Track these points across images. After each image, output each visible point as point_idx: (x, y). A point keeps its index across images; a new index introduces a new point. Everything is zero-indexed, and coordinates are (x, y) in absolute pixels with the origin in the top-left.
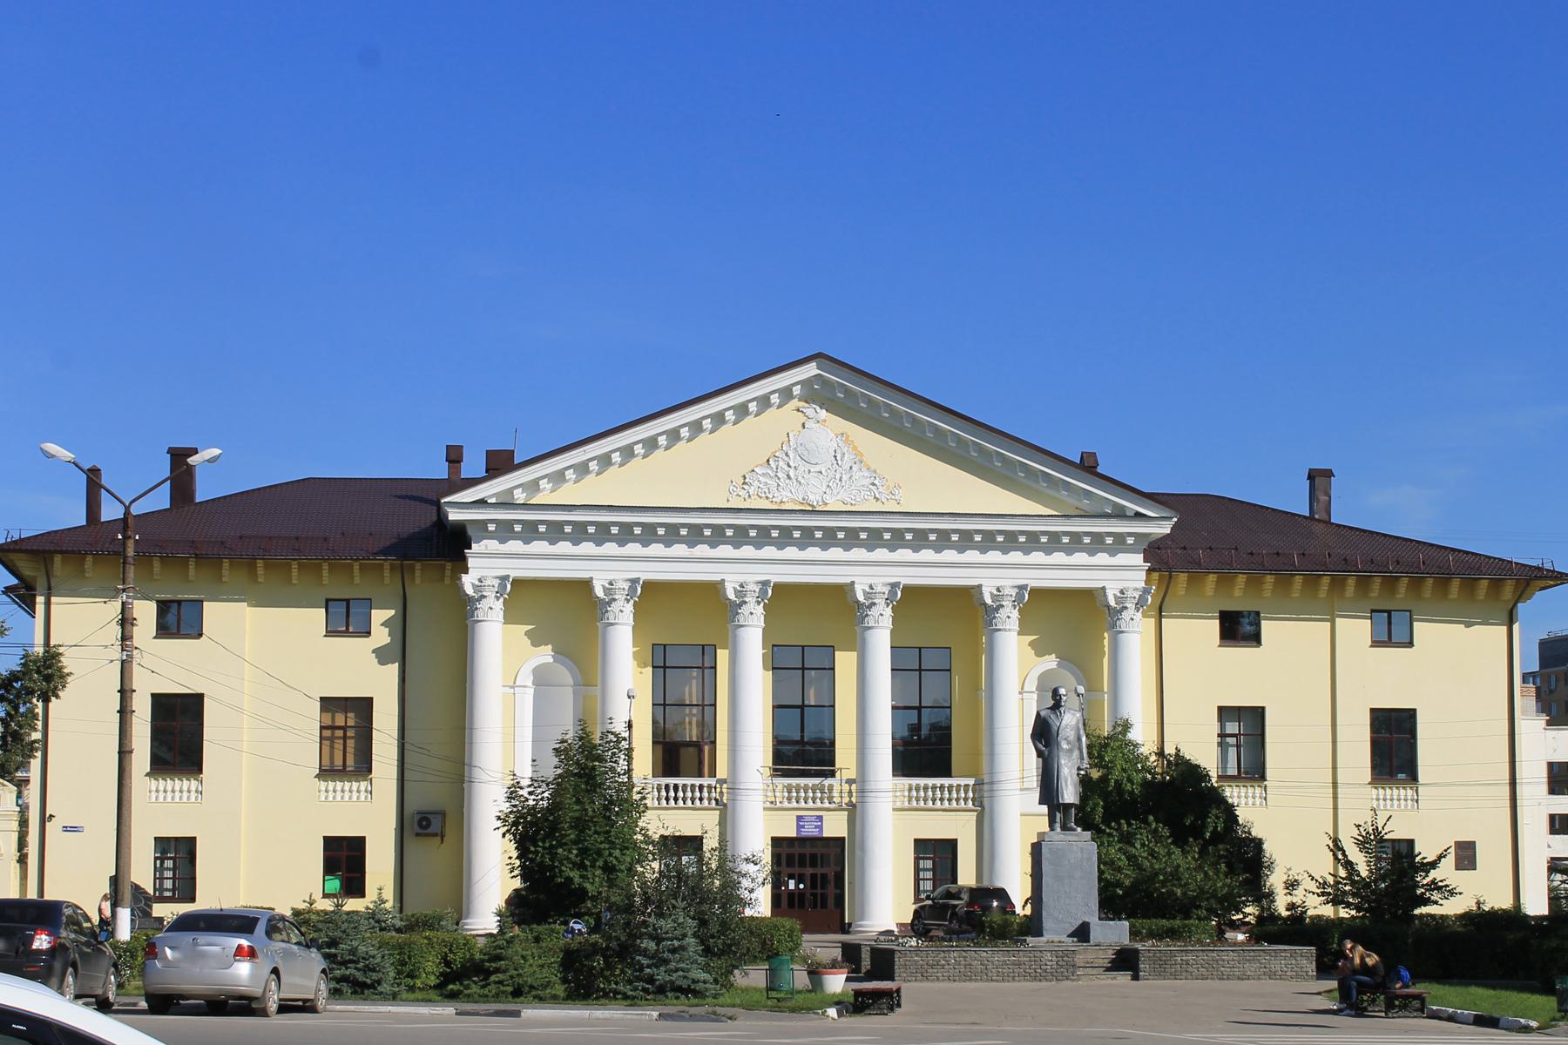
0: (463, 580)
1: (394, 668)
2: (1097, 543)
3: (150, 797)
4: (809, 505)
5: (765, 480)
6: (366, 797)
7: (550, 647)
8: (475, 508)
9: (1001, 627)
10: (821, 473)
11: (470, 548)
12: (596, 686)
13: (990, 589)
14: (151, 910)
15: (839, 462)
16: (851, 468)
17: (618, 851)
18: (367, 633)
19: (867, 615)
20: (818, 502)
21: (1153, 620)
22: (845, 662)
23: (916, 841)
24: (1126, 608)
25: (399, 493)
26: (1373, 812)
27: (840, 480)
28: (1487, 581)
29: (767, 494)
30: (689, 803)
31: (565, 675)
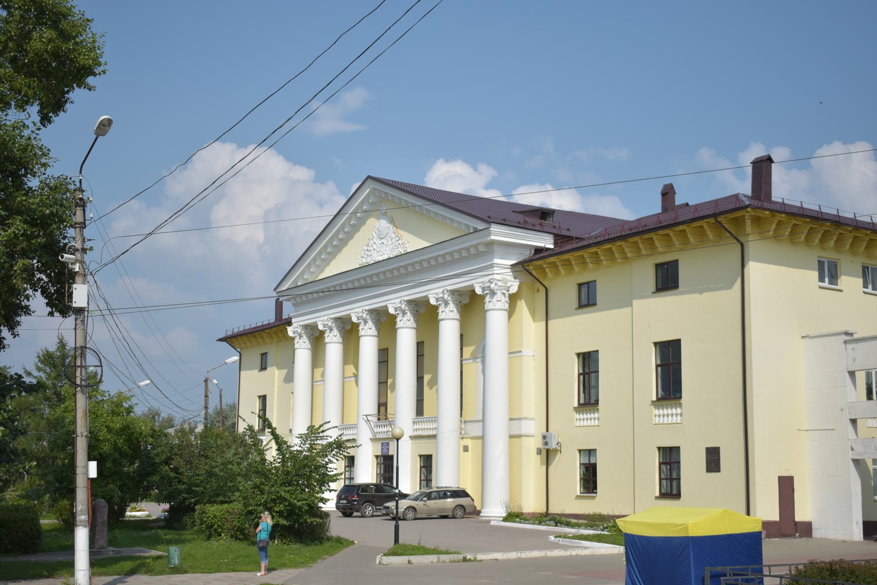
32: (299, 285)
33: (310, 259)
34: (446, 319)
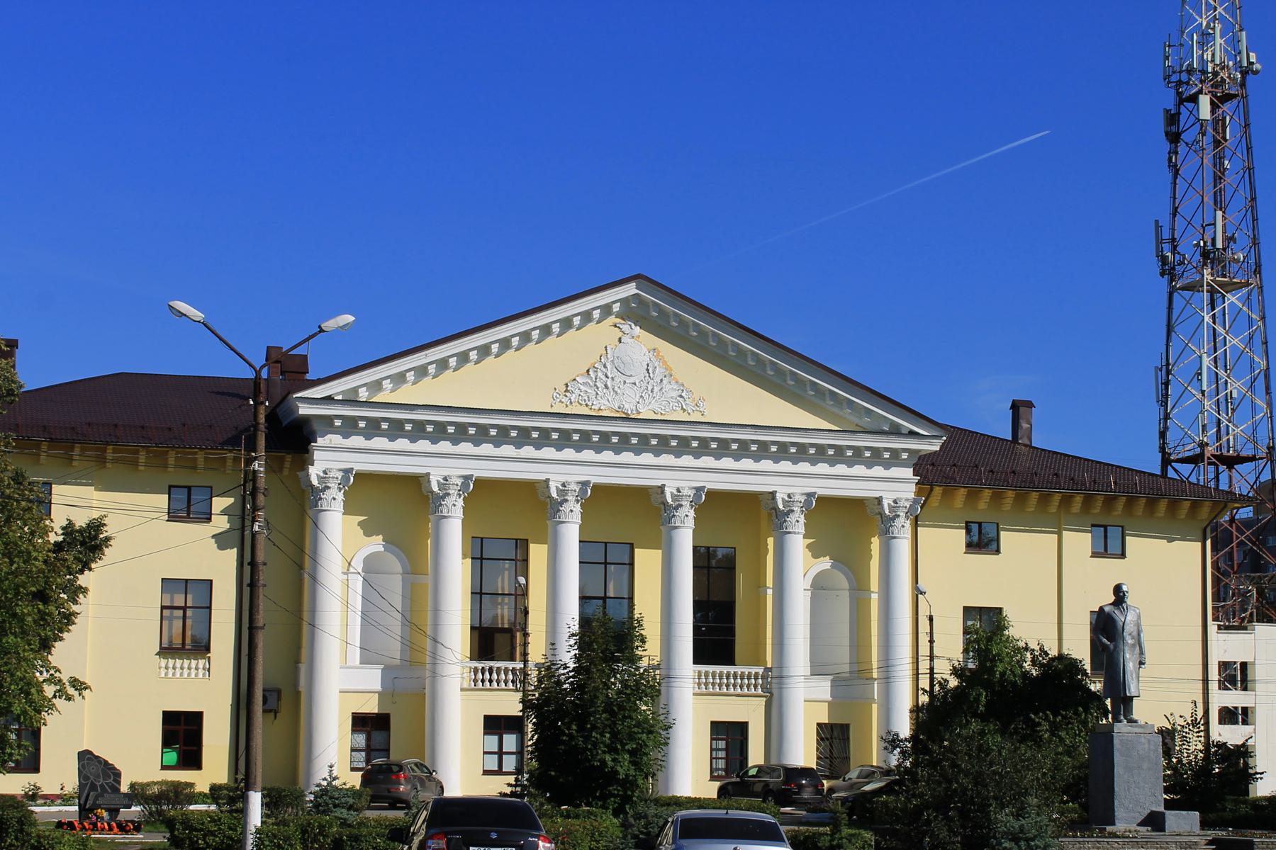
0: (310, 471)
1: (232, 553)
2: (876, 458)
3: (159, 672)
4: (624, 413)
5: (585, 389)
6: (204, 675)
7: (381, 537)
8: (324, 404)
9: (791, 530)
10: (635, 384)
11: (316, 442)
12: (427, 575)
13: (782, 496)
14: (120, 785)
15: (651, 375)
16: (661, 381)
17: (645, 735)
18: (207, 519)
19: (674, 516)
20: (632, 411)
21: (1200, 543)
22: (538, 554)
23: (712, 723)
24: (793, 511)
25: (215, 390)
26: (1193, 704)
27: (652, 392)
28: (1189, 502)
29: (587, 402)
30: (503, 685)
31: (395, 564)
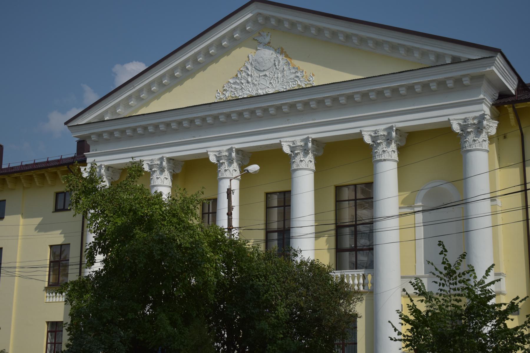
15: (277, 67)
32: (106, 119)
33: (134, 90)
34: (389, 160)
